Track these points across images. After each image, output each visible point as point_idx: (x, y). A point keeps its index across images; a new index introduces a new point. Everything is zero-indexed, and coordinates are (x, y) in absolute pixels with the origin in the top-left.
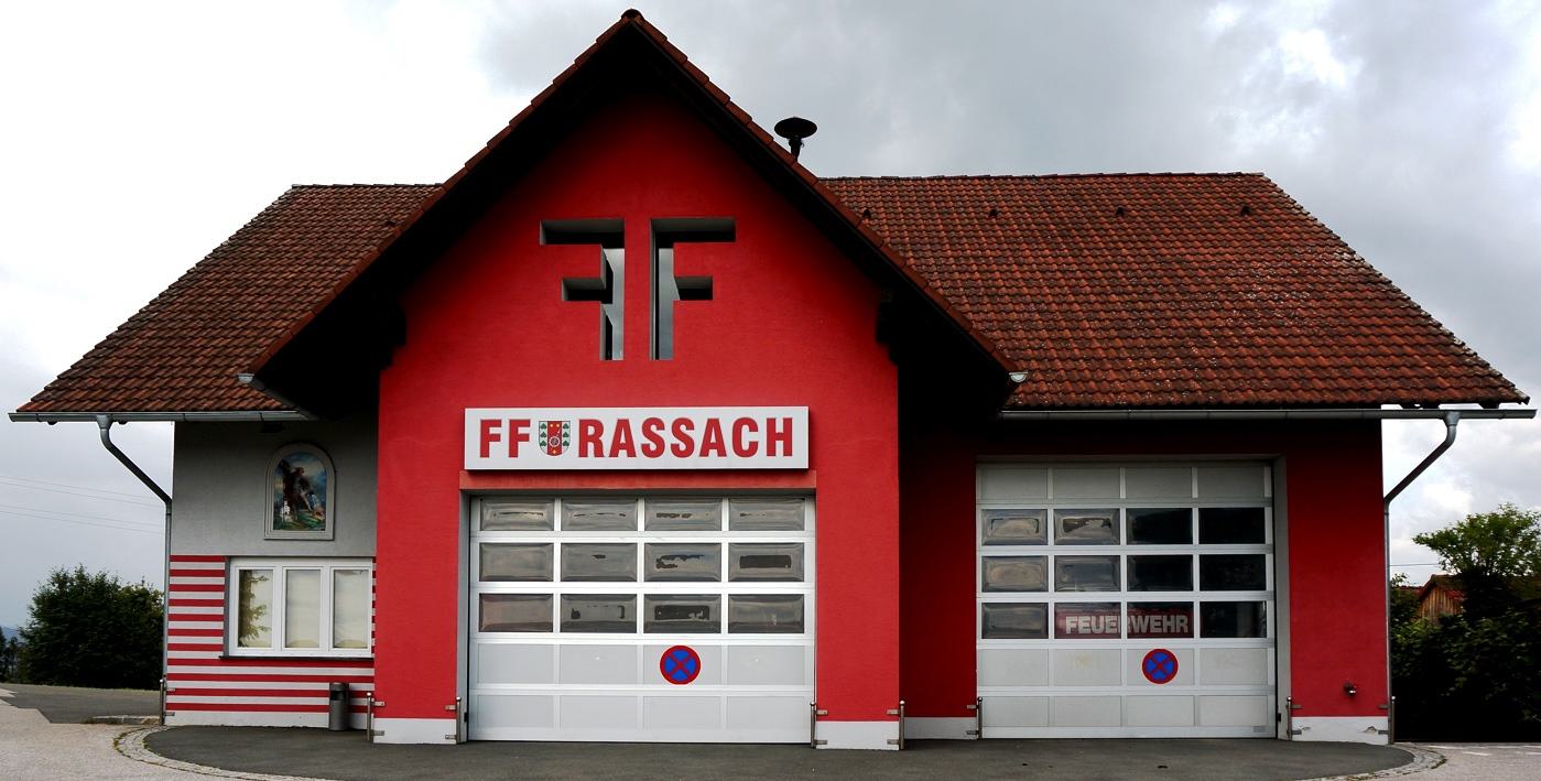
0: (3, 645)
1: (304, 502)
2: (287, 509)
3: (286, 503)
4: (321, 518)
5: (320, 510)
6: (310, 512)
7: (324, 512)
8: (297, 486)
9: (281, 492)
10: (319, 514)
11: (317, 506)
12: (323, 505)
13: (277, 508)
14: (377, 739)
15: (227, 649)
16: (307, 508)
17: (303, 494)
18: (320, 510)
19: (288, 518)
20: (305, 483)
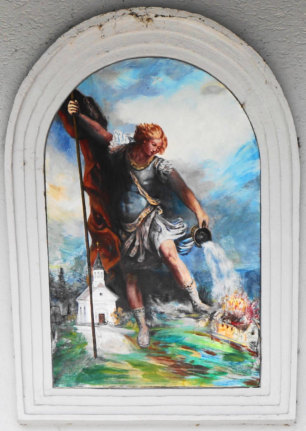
0: (134, 143)
1: (174, 272)
2: (105, 301)
3: (99, 276)
4: (243, 339)
5: (239, 304)
6: (197, 313)
7: (256, 313)
8: (140, 204)
9: (77, 232)
10: (234, 320)
11: (227, 289)
12: (252, 282)
13: (63, 296)
14: (241, 350)
15: (103, 326)
16: (183, 296)
17: (166, 239)
18: (239, 304)
19: (113, 341)
20: (172, 194)
